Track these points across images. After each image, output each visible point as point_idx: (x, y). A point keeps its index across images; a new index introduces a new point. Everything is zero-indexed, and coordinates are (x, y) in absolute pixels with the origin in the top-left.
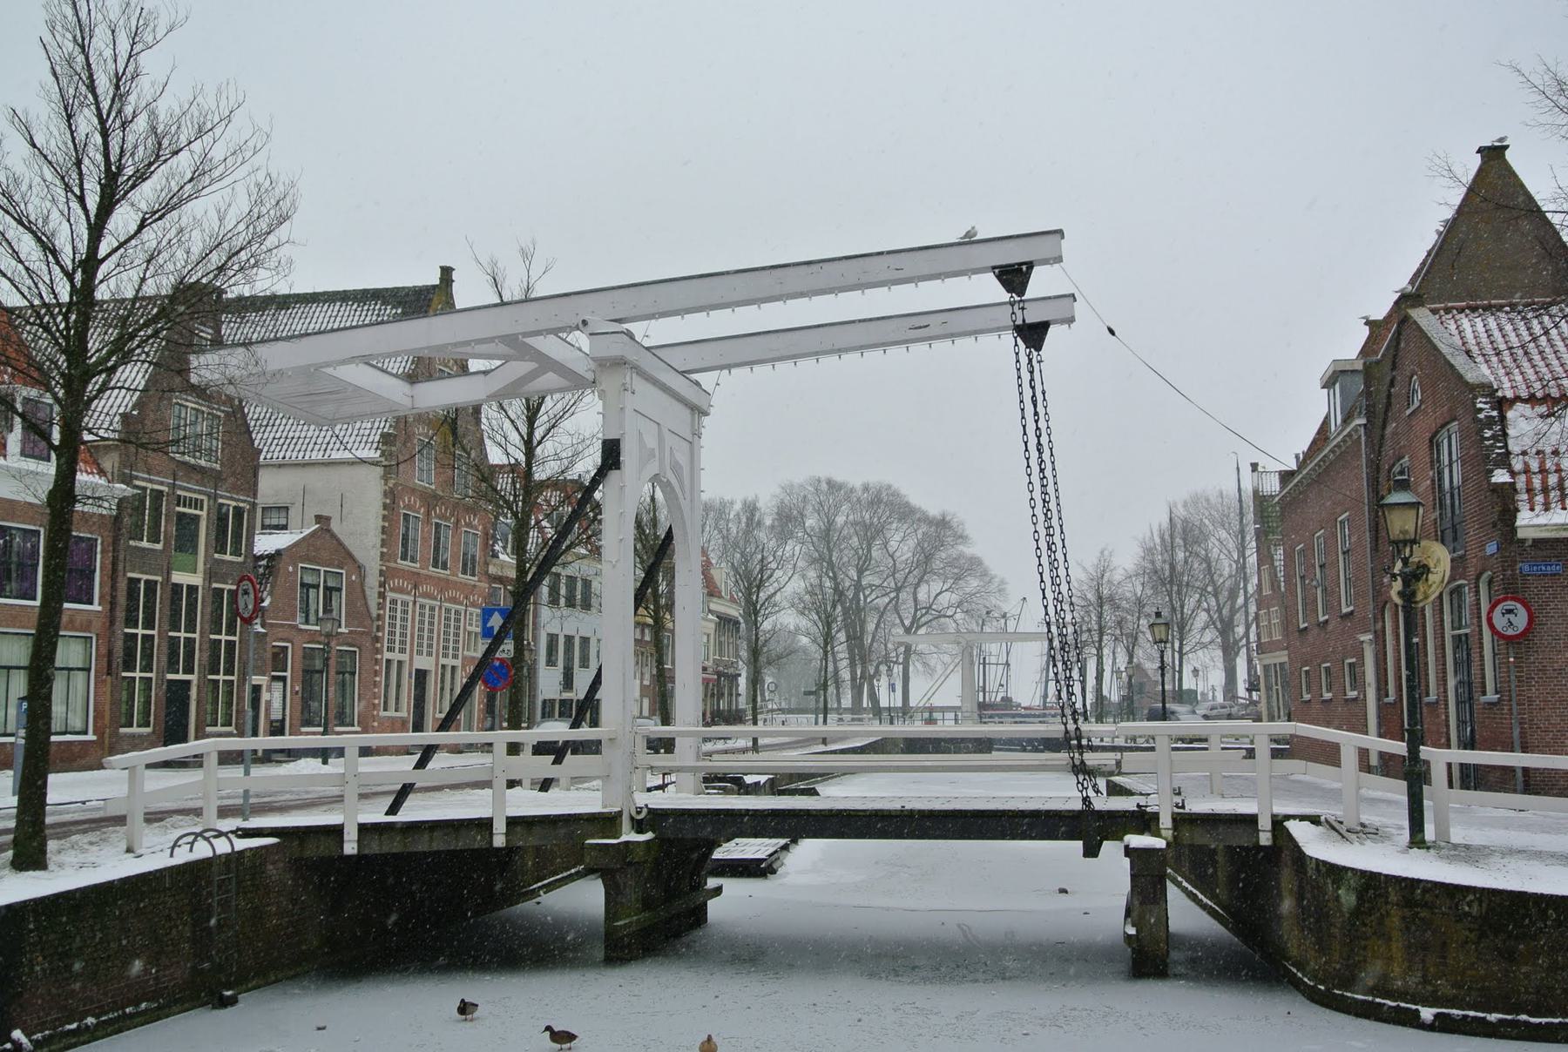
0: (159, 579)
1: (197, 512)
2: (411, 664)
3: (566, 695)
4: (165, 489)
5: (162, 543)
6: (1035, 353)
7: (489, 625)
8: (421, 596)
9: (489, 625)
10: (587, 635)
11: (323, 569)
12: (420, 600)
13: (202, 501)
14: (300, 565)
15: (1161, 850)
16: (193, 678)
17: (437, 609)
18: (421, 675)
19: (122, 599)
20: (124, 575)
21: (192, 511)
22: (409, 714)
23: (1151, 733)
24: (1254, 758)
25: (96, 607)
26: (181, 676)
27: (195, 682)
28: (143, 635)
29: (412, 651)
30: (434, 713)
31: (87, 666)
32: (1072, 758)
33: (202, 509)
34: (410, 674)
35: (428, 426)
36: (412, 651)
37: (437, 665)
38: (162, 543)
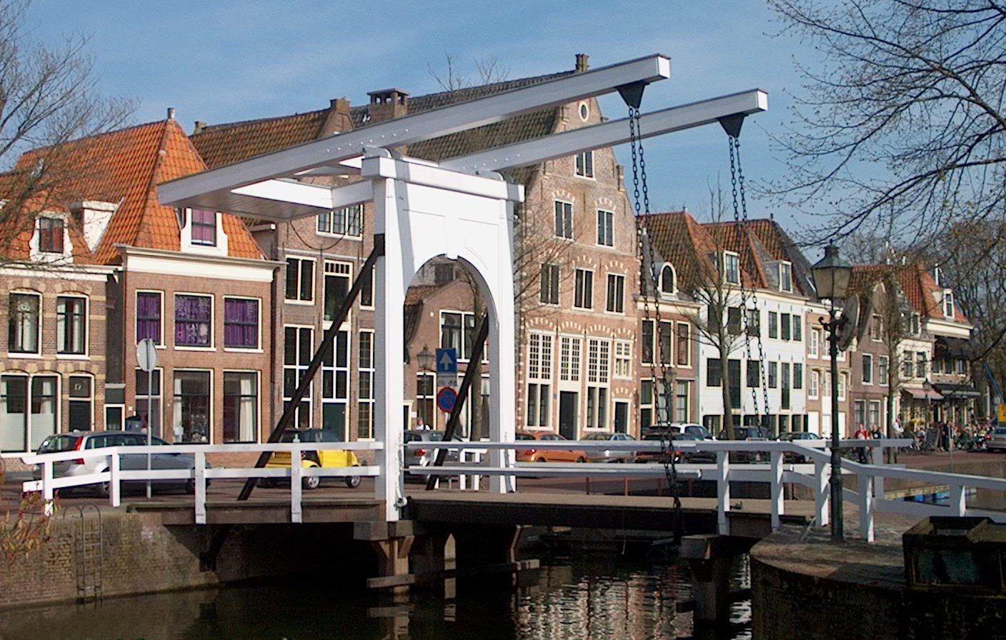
0: (313, 327)
1: (345, 275)
2: (555, 388)
3: (784, 412)
4: (315, 259)
5: (313, 300)
6: (734, 139)
7: (441, 362)
8: (563, 331)
9: (441, 362)
10: (787, 362)
11: (463, 313)
12: (562, 334)
13: (348, 266)
14: (441, 311)
15: (385, 518)
16: (346, 401)
17: (581, 341)
18: (568, 399)
19: (280, 342)
20: (281, 326)
21: (340, 274)
22: (555, 428)
23: (766, 450)
24: (194, 454)
25: (260, 350)
26: (335, 400)
27: (348, 405)
28: (337, 372)
29: (556, 377)
30: (582, 428)
31: (255, 394)
32: (667, 468)
33: (347, 272)
34: (555, 396)
35: (566, 189)
36: (556, 377)
37: (583, 388)
38: (313, 300)
